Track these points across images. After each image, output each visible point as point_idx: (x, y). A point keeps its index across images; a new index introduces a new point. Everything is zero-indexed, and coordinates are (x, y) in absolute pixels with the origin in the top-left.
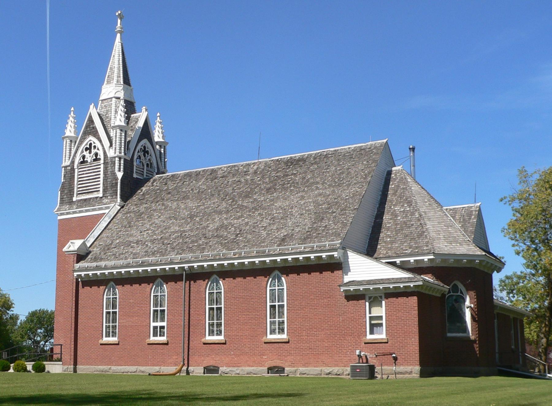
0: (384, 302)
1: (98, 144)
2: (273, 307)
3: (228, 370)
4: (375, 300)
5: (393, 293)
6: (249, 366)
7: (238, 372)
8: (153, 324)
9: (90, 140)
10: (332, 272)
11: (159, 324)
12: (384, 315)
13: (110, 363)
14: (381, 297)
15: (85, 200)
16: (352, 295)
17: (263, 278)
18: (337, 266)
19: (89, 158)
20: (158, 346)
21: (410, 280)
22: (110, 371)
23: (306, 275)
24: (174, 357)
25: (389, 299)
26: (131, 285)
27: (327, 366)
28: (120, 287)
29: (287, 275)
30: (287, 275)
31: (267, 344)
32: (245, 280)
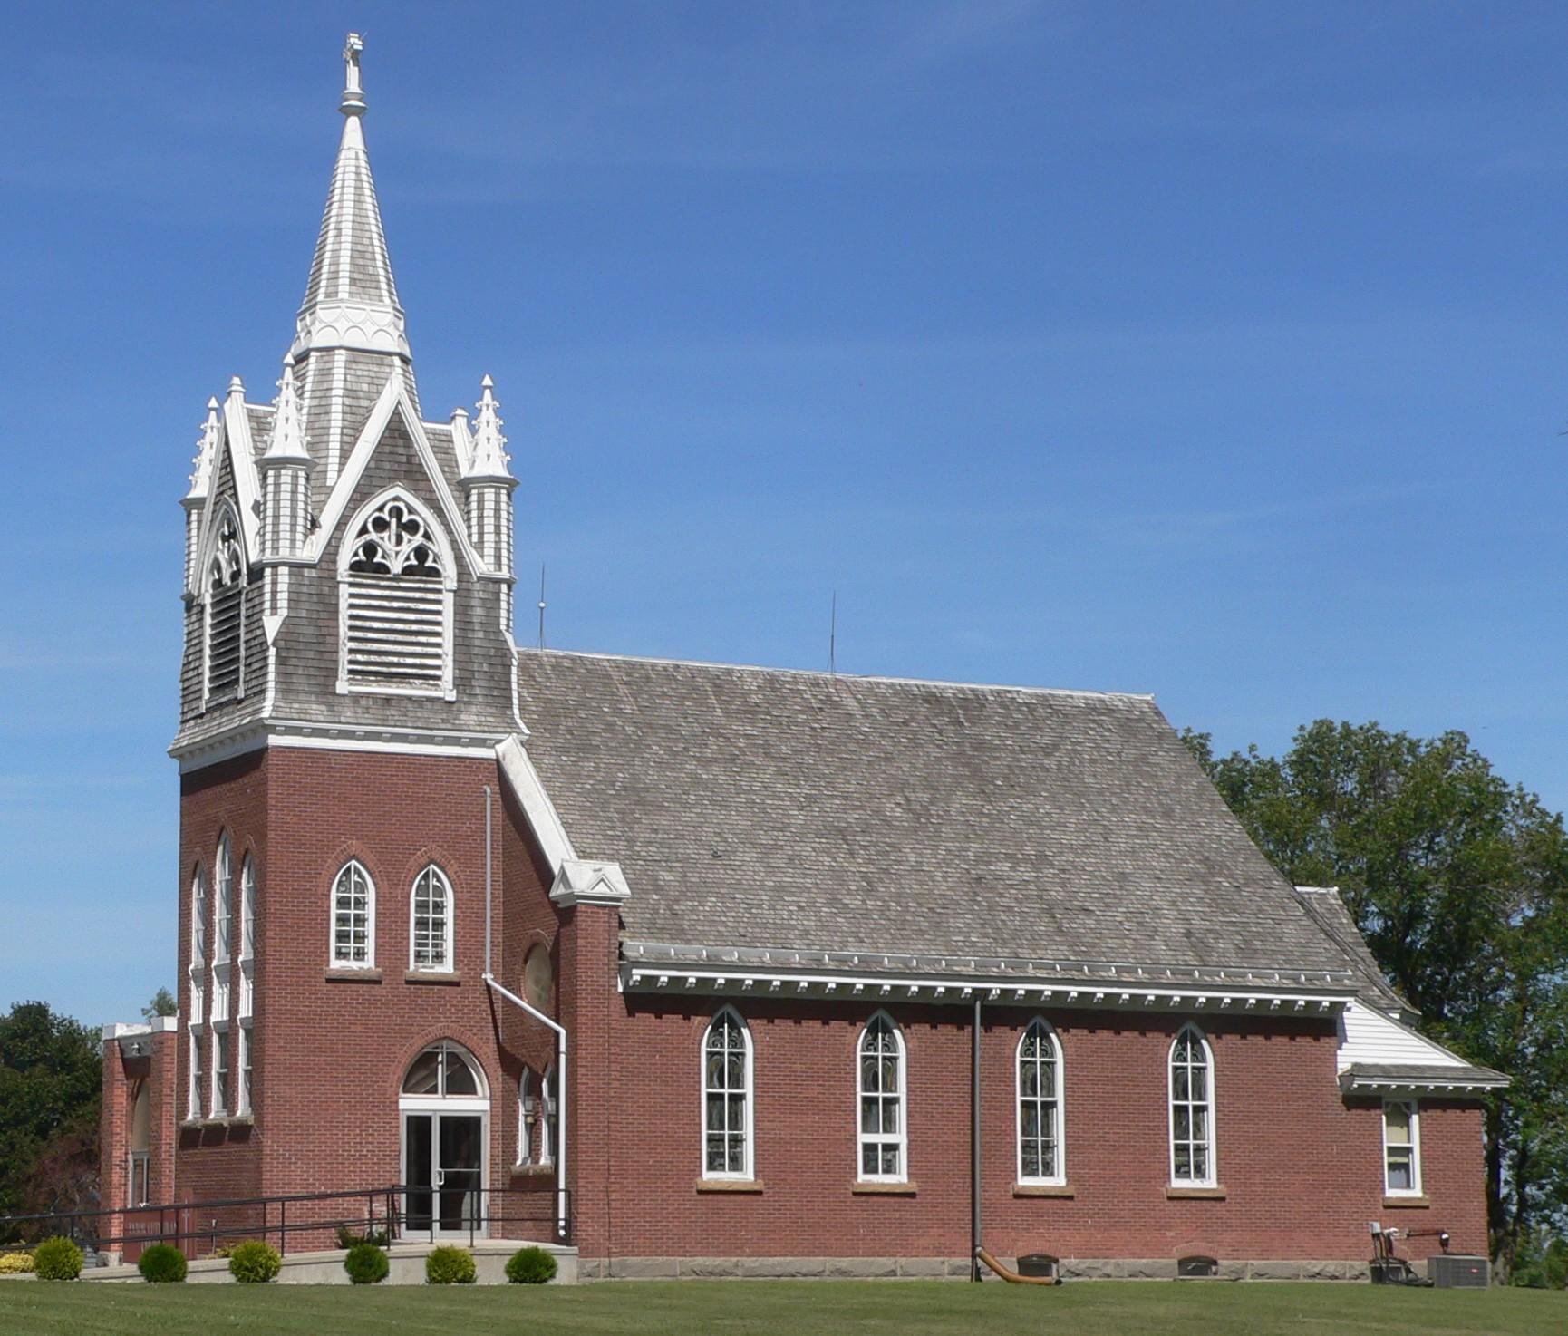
0: (1415, 1119)
1: (425, 514)
2: (1180, 1111)
3: (1083, 1266)
4: (1400, 1116)
5: (1434, 1102)
6: (1133, 1255)
7: (1108, 1270)
8: (863, 1138)
9: (396, 499)
10: (1317, 1039)
11: (880, 1138)
12: (1416, 1145)
13: (734, 1248)
15: (387, 700)
16: (1449, 1100)
17: (1161, 1036)
18: (1326, 1026)
19: (397, 556)
23: (1260, 1039)
24: (935, 1231)
25: (1430, 1112)
27: (1310, 1256)
30: (1219, 1037)
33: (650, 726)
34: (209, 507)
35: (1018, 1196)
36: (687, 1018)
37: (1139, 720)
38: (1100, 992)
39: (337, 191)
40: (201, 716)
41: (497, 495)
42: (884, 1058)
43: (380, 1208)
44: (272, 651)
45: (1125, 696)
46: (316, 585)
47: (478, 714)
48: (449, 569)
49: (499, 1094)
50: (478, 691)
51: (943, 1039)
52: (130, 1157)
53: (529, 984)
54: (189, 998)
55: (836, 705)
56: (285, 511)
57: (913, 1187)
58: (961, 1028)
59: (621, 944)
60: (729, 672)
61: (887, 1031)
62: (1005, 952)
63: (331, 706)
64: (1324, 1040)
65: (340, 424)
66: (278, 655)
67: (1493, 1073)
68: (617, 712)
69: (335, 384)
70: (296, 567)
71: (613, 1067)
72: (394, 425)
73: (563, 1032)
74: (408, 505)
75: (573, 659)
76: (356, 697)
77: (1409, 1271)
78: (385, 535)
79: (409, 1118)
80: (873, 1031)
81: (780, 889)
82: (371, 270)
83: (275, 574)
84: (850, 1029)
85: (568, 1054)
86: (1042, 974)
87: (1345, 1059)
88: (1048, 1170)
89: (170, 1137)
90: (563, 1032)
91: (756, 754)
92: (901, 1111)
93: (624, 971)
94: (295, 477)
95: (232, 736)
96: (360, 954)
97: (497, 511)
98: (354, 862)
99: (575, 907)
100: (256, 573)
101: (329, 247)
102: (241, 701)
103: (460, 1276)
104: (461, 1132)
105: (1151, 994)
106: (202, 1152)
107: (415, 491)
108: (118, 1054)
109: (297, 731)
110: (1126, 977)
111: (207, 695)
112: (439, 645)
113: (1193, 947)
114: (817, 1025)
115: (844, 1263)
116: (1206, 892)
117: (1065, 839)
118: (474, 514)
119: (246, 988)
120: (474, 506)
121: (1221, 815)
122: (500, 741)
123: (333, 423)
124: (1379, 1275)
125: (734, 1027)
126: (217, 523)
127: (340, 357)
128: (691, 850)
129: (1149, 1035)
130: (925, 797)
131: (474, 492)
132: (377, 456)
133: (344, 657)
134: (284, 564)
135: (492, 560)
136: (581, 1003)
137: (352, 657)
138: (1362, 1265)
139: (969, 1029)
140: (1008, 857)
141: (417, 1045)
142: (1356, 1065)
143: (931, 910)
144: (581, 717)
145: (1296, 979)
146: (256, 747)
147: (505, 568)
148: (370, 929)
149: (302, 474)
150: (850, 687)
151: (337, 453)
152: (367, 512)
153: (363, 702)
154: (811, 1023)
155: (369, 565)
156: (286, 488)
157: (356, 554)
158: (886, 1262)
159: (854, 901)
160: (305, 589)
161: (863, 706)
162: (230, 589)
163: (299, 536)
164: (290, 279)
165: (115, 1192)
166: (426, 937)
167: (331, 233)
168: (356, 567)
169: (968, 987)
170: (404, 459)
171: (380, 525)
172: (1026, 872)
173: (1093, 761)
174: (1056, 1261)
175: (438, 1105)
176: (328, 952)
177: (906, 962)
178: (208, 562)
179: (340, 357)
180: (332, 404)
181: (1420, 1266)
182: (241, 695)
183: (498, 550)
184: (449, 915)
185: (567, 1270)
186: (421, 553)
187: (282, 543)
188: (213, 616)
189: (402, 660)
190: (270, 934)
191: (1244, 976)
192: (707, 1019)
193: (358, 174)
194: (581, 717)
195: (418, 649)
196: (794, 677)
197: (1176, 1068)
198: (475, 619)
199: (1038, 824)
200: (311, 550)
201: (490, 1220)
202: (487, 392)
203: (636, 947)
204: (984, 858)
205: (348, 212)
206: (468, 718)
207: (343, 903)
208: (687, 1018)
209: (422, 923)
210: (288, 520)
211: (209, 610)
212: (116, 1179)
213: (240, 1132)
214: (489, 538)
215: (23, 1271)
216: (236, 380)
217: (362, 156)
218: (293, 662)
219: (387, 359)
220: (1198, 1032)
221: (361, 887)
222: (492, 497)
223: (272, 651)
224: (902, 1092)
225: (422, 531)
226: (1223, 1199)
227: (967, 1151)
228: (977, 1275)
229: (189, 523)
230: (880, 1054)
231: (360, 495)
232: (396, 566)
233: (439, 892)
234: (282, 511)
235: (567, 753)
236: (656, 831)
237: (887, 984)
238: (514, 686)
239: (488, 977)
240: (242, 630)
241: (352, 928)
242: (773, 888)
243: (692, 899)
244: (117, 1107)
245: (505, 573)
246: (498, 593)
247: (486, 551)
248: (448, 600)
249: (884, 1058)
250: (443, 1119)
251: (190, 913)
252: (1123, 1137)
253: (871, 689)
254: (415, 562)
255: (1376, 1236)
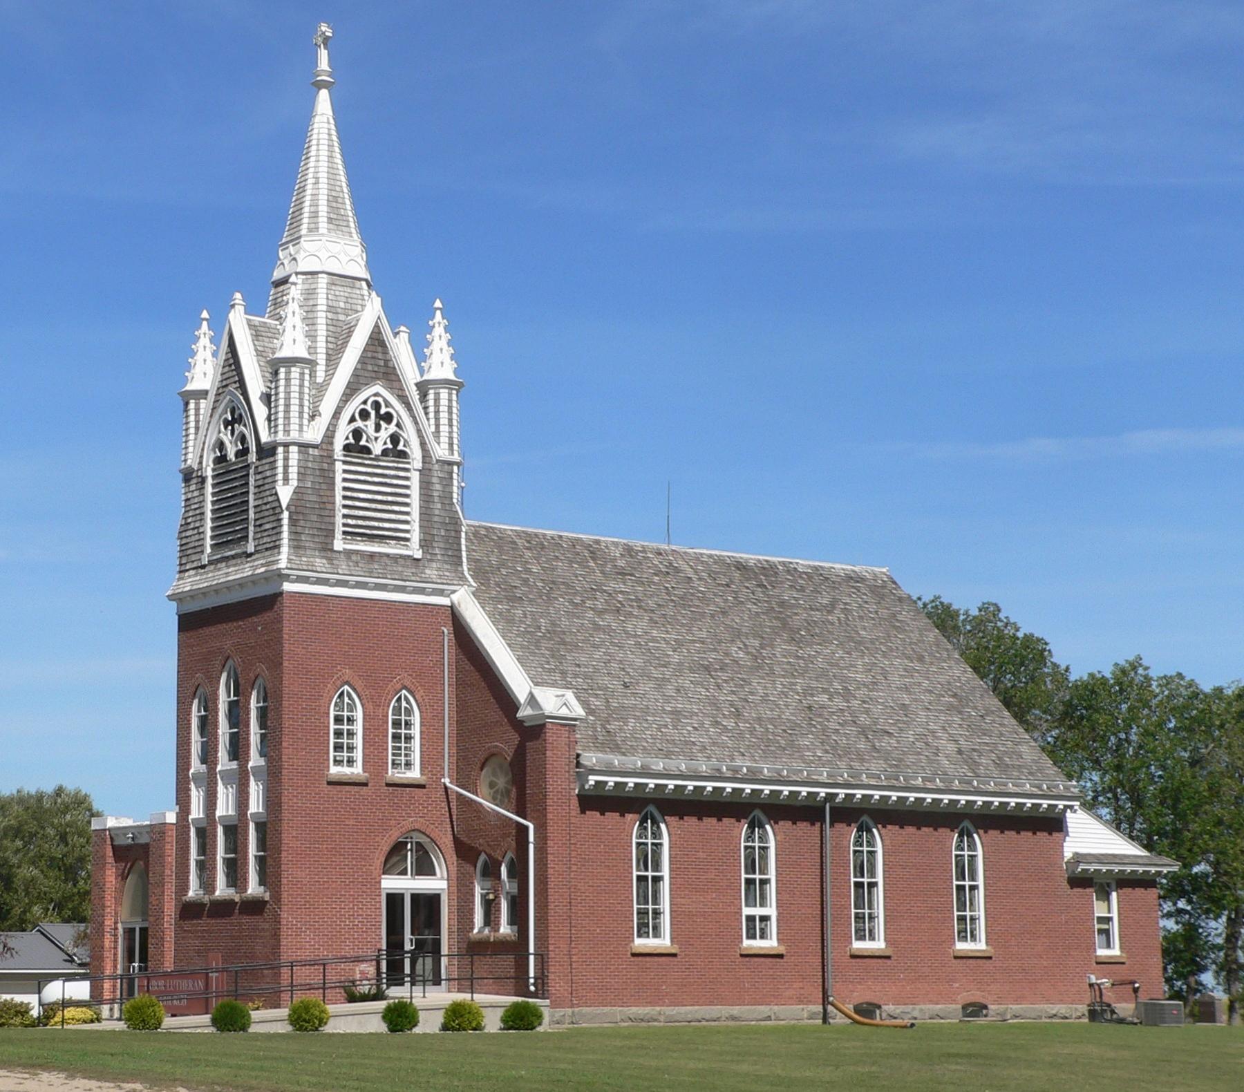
0: (1114, 894)
1: (398, 408)
6: (931, 1002)
7: (916, 1014)
9: (376, 395)
11: (757, 911)
12: (1115, 914)
14: (1108, 885)
15: (372, 556)
18: (1054, 824)
20: (762, 959)
21: (1132, 860)
22: (662, 1018)
24: (796, 985)
25: (1125, 890)
26: (1018, 833)
27: (1048, 1001)
28: (671, 820)
29: (776, 823)
31: (958, 961)
32: (920, 832)
33: (554, 582)
34: (211, 397)
35: (853, 957)
36: (622, 815)
37: (883, 587)
38: (912, 796)
39: (314, 148)
40: (203, 567)
41: (450, 394)
42: (760, 848)
43: (370, 969)
44: (286, 515)
45: (869, 568)
46: (318, 461)
47: (438, 569)
48: (416, 453)
49: (454, 876)
50: (437, 551)
51: (801, 833)
52: (119, 925)
53: (484, 787)
54: (189, 796)
55: (677, 570)
56: (295, 401)
57: (782, 950)
58: (812, 824)
59: (578, 756)
60: (597, 542)
61: (762, 826)
62: (842, 764)
63: (330, 560)
64: (1055, 835)
65: (325, 333)
66: (290, 518)
67: (1166, 860)
68: (529, 571)
69: (319, 302)
70: (303, 447)
71: (574, 854)
72: (375, 336)
73: (531, 827)
74: (385, 400)
75: (486, 528)
76: (348, 553)
77: (1113, 1012)
78: (368, 423)
79: (388, 895)
80: (752, 827)
81: (676, 713)
82: (342, 212)
83: (286, 452)
84: (847, 828)
85: (528, 843)
86: (873, 782)
87: (1071, 847)
88: (657, 933)
89: (170, 910)
90: (531, 827)
91: (632, 606)
92: (772, 889)
93: (582, 778)
94: (302, 374)
95: (254, 580)
96: (351, 762)
97: (450, 407)
98: (346, 687)
99: (544, 725)
100: (267, 452)
101: (309, 192)
102: (251, 555)
103: (474, 1025)
104: (427, 905)
105: (946, 798)
106: (204, 923)
107: (390, 389)
108: (109, 842)
109: (305, 580)
110: (929, 785)
111: (209, 550)
112: (407, 513)
113: (966, 762)
114: (713, 821)
115: (735, 1010)
116: (962, 719)
117: (859, 677)
118: (431, 409)
119: (256, 792)
120: (431, 403)
121: (957, 662)
122: (454, 592)
123: (319, 333)
124: (1093, 1015)
125: (655, 823)
126: (220, 410)
127: (323, 280)
128: (606, 680)
129: (940, 830)
130: (756, 643)
131: (431, 391)
132: (363, 360)
133: (339, 521)
134: (294, 444)
135: (447, 446)
136: (549, 802)
137: (345, 521)
138: (1083, 1008)
139: (818, 825)
140: (825, 691)
141: (394, 836)
142: (1076, 854)
143: (784, 731)
144: (509, 569)
145: (1040, 788)
146: (272, 592)
147: (456, 453)
148: (358, 741)
149: (307, 371)
150: (684, 556)
151: (324, 356)
152: (354, 406)
153: (354, 558)
154: (710, 819)
155: (356, 448)
156: (295, 382)
157: (347, 438)
158: (764, 1010)
159: (730, 723)
160: (310, 465)
161: (696, 572)
162: (234, 464)
163: (305, 422)
164: (276, 220)
165: (107, 954)
166: (400, 748)
167: (311, 181)
168: (347, 448)
169: (823, 792)
170: (382, 363)
171: (364, 415)
172: (839, 703)
173: (861, 618)
174: (879, 1007)
175: (406, 884)
176: (328, 760)
177: (779, 772)
178: (211, 440)
179: (323, 280)
180: (321, 315)
181: (1125, 1008)
182: (251, 548)
183: (451, 438)
184: (416, 731)
185: (551, 1018)
186: (395, 439)
187: (292, 427)
188: (214, 486)
189: (381, 525)
190: (285, 744)
191: (1005, 785)
192: (637, 816)
193: (329, 135)
194: (509, 569)
195: (393, 516)
196: (643, 547)
197: (957, 856)
198: (435, 494)
199: (837, 665)
200: (314, 433)
201: (448, 980)
202: (205, 323)
203: (590, 758)
204: (808, 692)
205: (324, 164)
206: (431, 573)
207: (338, 720)
208: (622, 815)
209: (396, 737)
210: (297, 408)
211: (210, 481)
212: (107, 943)
213: (254, 907)
214: (444, 429)
215: (85, 1022)
216: (238, 296)
217: (332, 121)
218: (302, 523)
219: (358, 284)
220: (871, 823)
221: (351, 708)
222: (446, 396)
223: (286, 515)
224: (772, 875)
225: (395, 422)
226: (990, 958)
227: (820, 918)
228: (825, 1019)
229: (186, 410)
230: (650, 841)
231: (351, 390)
232: (377, 449)
233: (409, 712)
234: (292, 401)
235: (501, 602)
236: (579, 666)
237: (767, 789)
238: (464, 548)
239: (447, 781)
240: (251, 497)
241: (345, 741)
242: (671, 713)
243: (617, 720)
244: (108, 885)
245: (456, 457)
246: (452, 473)
247: (442, 439)
248: (415, 477)
249: (653, 844)
250: (413, 896)
251: (189, 727)
252: (927, 910)
253: (698, 558)
254: (390, 446)
255: (1091, 985)
